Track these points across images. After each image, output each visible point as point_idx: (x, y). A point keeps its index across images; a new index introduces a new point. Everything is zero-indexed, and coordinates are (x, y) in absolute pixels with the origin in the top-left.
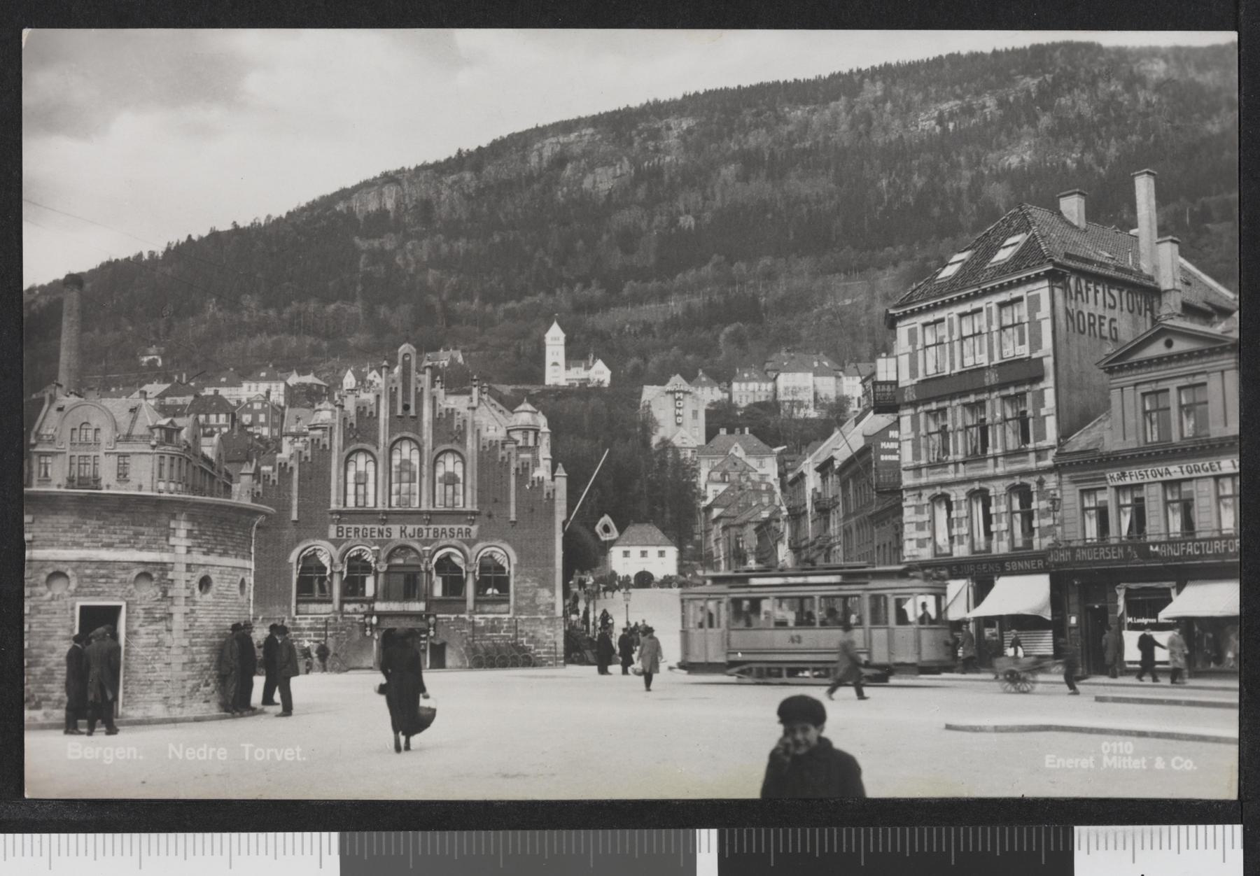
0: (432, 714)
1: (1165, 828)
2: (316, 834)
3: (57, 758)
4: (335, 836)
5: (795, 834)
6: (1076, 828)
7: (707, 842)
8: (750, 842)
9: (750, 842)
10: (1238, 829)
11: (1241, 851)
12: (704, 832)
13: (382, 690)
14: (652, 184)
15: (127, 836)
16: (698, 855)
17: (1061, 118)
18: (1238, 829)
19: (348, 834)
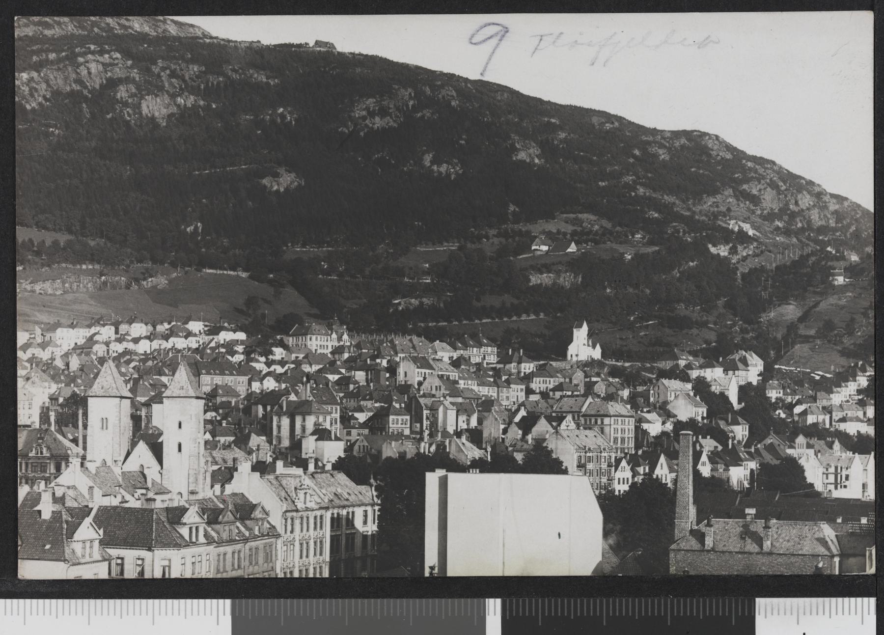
0: (759, 375)
1: (827, 600)
2: (214, 601)
3: (30, 569)
4: (228, 602)
5: (563, 603)
6: (757, 600)
7: (494, 608)
8: (614, 607)
9: (614, 607)
10: (873, 601)
11: (875, 617)
12: (491, 601)
13: (340, 458)
14: (236, 47)
15: (79, 601)
16: (488, 617)
17: (221, 318)
18: (873, 601)
19: (237, 601)
